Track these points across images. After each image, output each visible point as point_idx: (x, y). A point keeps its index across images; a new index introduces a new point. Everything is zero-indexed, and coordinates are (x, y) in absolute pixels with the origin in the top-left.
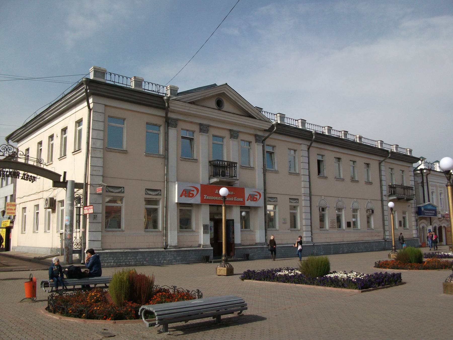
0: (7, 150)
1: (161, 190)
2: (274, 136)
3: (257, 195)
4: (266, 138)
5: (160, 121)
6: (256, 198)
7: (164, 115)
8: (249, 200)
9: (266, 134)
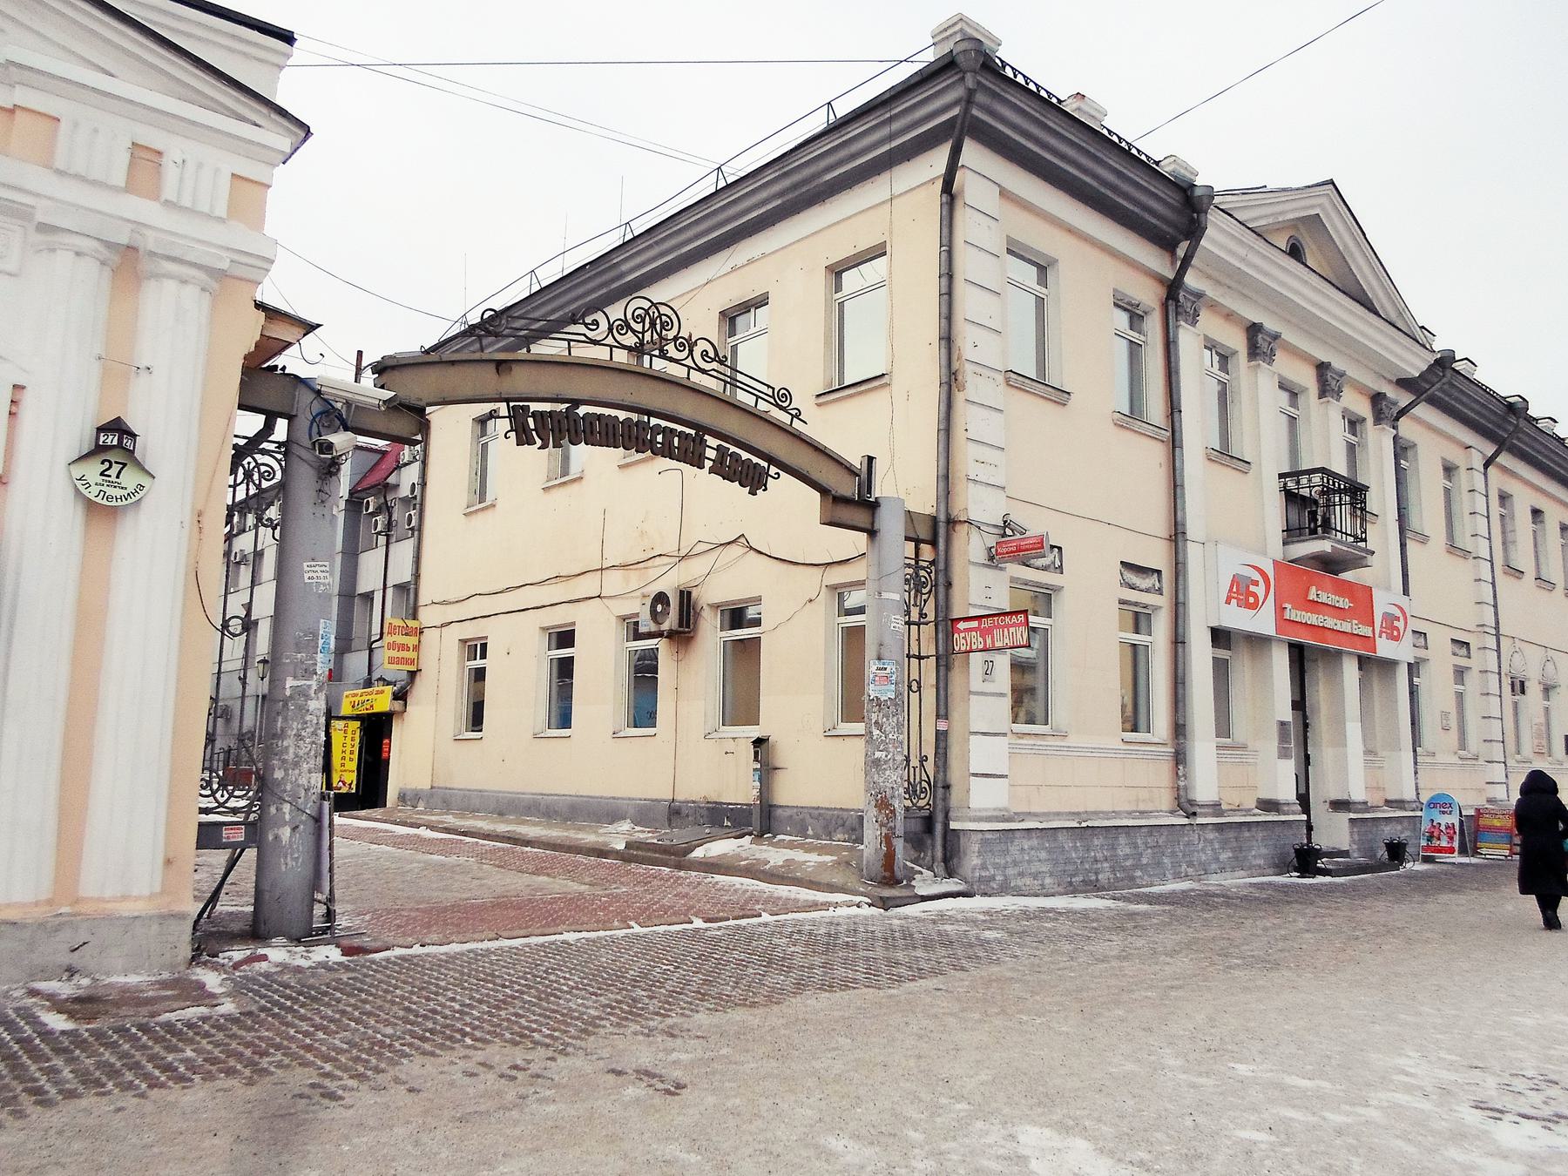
0: (653, 324)
1: (1159, 572)
2: (1423, 411)
3: (1256, 583)
4: (1403, 412)
5: (1148, 295)
6: (1255, 595)
7: (1171, 276)
8: (1234, 602)
9: (1404, 399)
